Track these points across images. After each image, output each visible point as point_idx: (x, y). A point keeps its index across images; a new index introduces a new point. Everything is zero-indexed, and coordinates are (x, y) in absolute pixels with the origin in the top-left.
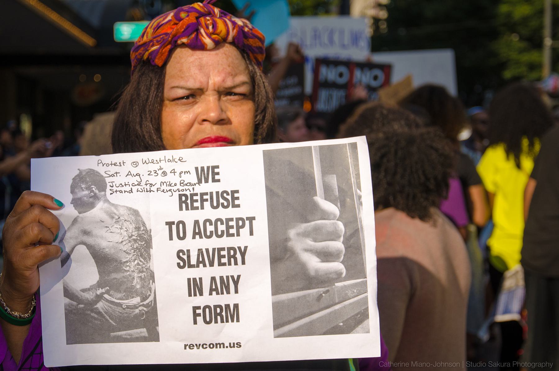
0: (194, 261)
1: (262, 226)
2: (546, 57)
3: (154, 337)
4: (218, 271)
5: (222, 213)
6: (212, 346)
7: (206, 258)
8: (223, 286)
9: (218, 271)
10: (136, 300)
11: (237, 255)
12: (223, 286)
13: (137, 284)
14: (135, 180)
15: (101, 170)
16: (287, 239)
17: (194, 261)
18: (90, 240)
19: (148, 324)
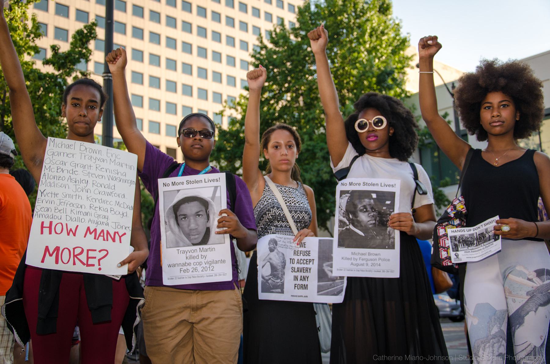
0: (296, 271)
1: (316, 262)
2: (335, 239)
3: (282, 292)
4: (303, 274)
5: (306, 257)
6: (299, 296)
7: (299, 270)
8: (304, 278)
9: (303, 274)
10: (279, 281)
11: (308, 270)
12: (304, 278)
13: (280, 276)
14: (284, 244)
15: (277, 239)
16: (323, 266)
17: (296, 271)
18: (271, 261)
19: (281, 288)
